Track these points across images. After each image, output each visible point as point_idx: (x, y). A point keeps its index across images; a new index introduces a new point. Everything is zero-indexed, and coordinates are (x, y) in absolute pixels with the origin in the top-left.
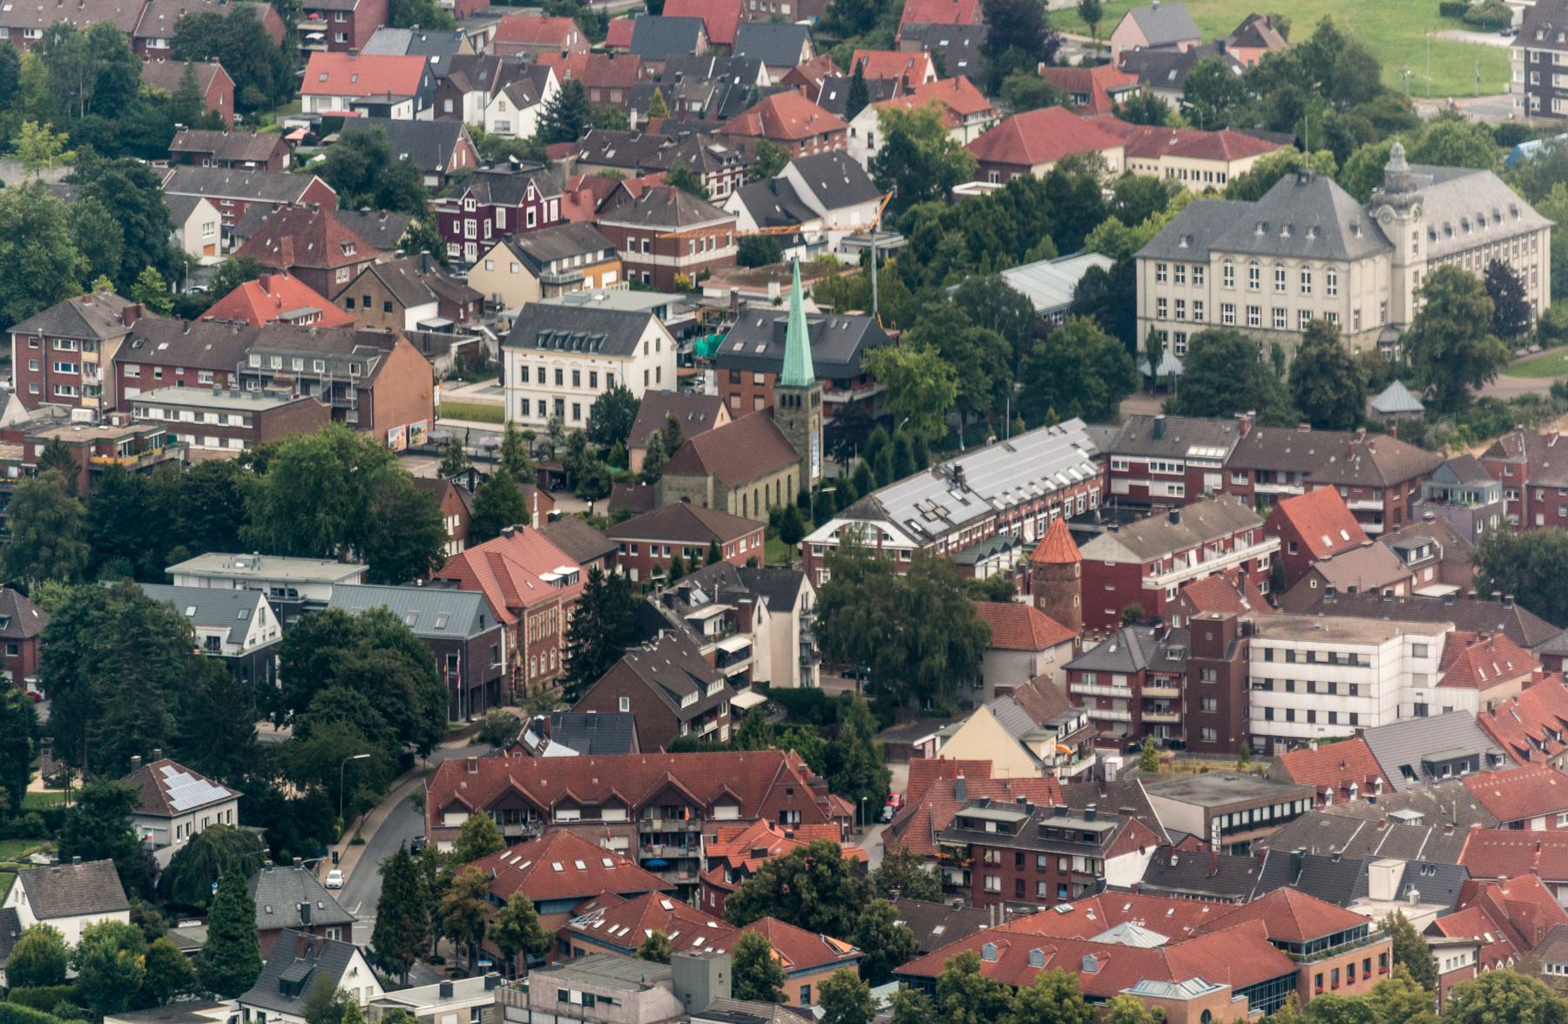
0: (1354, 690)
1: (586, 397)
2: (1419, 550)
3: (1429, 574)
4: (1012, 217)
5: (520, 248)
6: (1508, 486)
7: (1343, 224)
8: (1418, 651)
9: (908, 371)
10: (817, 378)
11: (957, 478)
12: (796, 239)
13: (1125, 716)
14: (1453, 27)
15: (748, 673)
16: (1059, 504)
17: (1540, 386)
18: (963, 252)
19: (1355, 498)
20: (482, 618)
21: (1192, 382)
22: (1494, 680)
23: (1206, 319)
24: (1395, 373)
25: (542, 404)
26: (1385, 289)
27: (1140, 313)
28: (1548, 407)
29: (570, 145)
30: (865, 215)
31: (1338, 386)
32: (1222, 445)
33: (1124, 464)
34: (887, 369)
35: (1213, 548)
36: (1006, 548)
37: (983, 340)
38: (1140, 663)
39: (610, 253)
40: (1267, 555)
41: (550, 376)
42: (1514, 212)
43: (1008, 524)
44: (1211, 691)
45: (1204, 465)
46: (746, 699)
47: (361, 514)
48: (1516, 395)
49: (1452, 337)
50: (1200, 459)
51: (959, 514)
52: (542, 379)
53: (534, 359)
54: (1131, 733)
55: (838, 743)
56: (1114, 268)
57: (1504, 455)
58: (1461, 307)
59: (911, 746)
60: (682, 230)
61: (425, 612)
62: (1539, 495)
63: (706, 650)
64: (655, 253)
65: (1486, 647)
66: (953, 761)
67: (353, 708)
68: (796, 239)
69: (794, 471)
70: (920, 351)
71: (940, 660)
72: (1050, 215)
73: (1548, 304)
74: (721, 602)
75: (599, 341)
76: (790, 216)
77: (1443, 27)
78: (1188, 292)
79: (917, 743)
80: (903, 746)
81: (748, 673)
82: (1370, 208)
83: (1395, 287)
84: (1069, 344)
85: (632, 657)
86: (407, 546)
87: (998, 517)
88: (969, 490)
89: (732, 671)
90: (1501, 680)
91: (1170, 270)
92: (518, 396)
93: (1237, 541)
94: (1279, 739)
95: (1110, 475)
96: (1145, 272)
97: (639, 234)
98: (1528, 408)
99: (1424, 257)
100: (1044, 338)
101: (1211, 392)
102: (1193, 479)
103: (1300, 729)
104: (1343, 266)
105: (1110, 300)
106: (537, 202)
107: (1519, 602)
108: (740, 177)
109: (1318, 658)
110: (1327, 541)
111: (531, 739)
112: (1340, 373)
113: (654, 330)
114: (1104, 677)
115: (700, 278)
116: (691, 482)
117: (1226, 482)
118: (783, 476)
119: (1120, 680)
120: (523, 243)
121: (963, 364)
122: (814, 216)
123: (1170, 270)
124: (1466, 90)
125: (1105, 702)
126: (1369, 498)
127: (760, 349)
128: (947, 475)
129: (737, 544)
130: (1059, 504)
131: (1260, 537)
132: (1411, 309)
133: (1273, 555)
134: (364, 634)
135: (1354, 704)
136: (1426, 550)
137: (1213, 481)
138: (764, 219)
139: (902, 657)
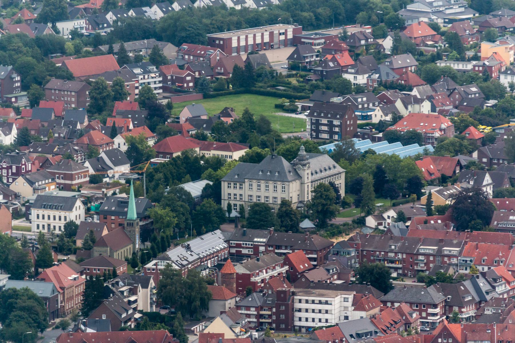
0: (327, 312)
1: (62, 223)
2: (333, 269)
3: (335, 277)
4: (174, 169)
5: (26, 178)
6: (357, 250)
7: (287, 171)
8: (346, 300)
9: (161, 215)
10: (138, 217)
11: (188, 248)
12: (106, 176)
13: (255, 320)
14: (280, 112)
15: (136, 307)
16: (217, 256)
17: (349, 220)
18: (162, 179)
19: (308, 254)
20: (54, 291)
21: (251, 218)
22: (370, 309)
23: (243, 200)
24: (304, 217)
25: (43, 226)
26: (299, 190)
27: (222, 198)
28: (352, 227)
29: (27, 147)
30: (125, 169)
31: (292, 220)
32: (265, 238)
33: (234, 243)
34: (155, 215)
35: (269, 269)
36: (205, 269)
37: (182, 206)
38: (259, 304)
39: (53, 180)
40: (285, 271)
41: (46, 217)
42: (334, 167)
43: (203, 262)
44: (282, 312)
45: (259, 244)
46: (137, 316)
47: (6, 259)
48: (341, 223)
49: (323, 205)
50: (258, 242)
51: (191, 259)
52: (43, 218)
53: (41, 212)
54: (257, 325)
55: (174, 328)
56: (213, 184)
57: (354, 241)
58: (326, 196)
59: (190, 330)
60: (73, 173)
61: (40, 289)
62: (365, 253)
63: (126, 300)
64: (65, 180)
65: (367, 298)
66: (213, 333)
67: (24, 318)
68: (106, 176)
69: (131, 246)
70: (165, 209)
71: (198, 303)
72: (185, 168)
73: (344, 195)
74: (128, 285)
75: (62, 206)
76: (103, 168)
77: (277, 112)
78: (238, 192)
79: (192, 329)
80: (188, 329)
81: (136, 307)
82: (294, 166)
83: (302, 190)
84: (207, 207)
85: (106, 302)
86: (21, 269)
87: (201, 260)
88: (192, 251)
89: (133, 306)
90: (372, 309)
91: (232, 185)
92: (36, 223)
93: (276, 267)
94: (303, 327)
95: (230, 247)
96: (224, 185)
97: (60, 174)
98: (346, 227)
99: (310, 181)
100: (200, 205)
101: (257, 221)
102: (256, 248)
103: (310, 324)
104: (287, 183)
105: (213, 192)
106: (25, 164)
107: (371, 285)
108: (83, 156)
109: (315, 302)
110: (302, 267)
111: (83, 327)
112: (292, 216)
113: (79, 203)
114: (248, 308)
115: (79, 188)
116: (104, 249)
117: (266, 249)
118: (128, 247)
119: (253, 309)
120: (27, 177)
121: (177, 213)
122: (111, 169)
123: (232, 185)
124: (290, 131)
125: (248, 316)
126: (312, 254)
127: (113, 208)
128: (185, 247)
129: (120, 268)
130: (217, 256)
131: (282, 267)
132: (308, 197)
133: (287, 271)
134: (23, 295)
135: (327, 316)
136: (335, 269)
137: (262, 249)
138: (96, 169)
139: (186, 302)
